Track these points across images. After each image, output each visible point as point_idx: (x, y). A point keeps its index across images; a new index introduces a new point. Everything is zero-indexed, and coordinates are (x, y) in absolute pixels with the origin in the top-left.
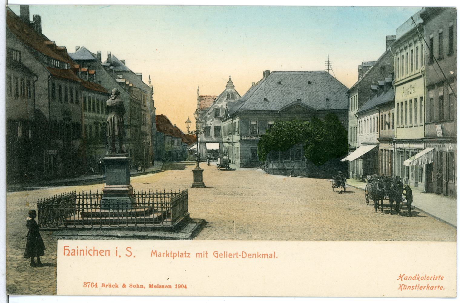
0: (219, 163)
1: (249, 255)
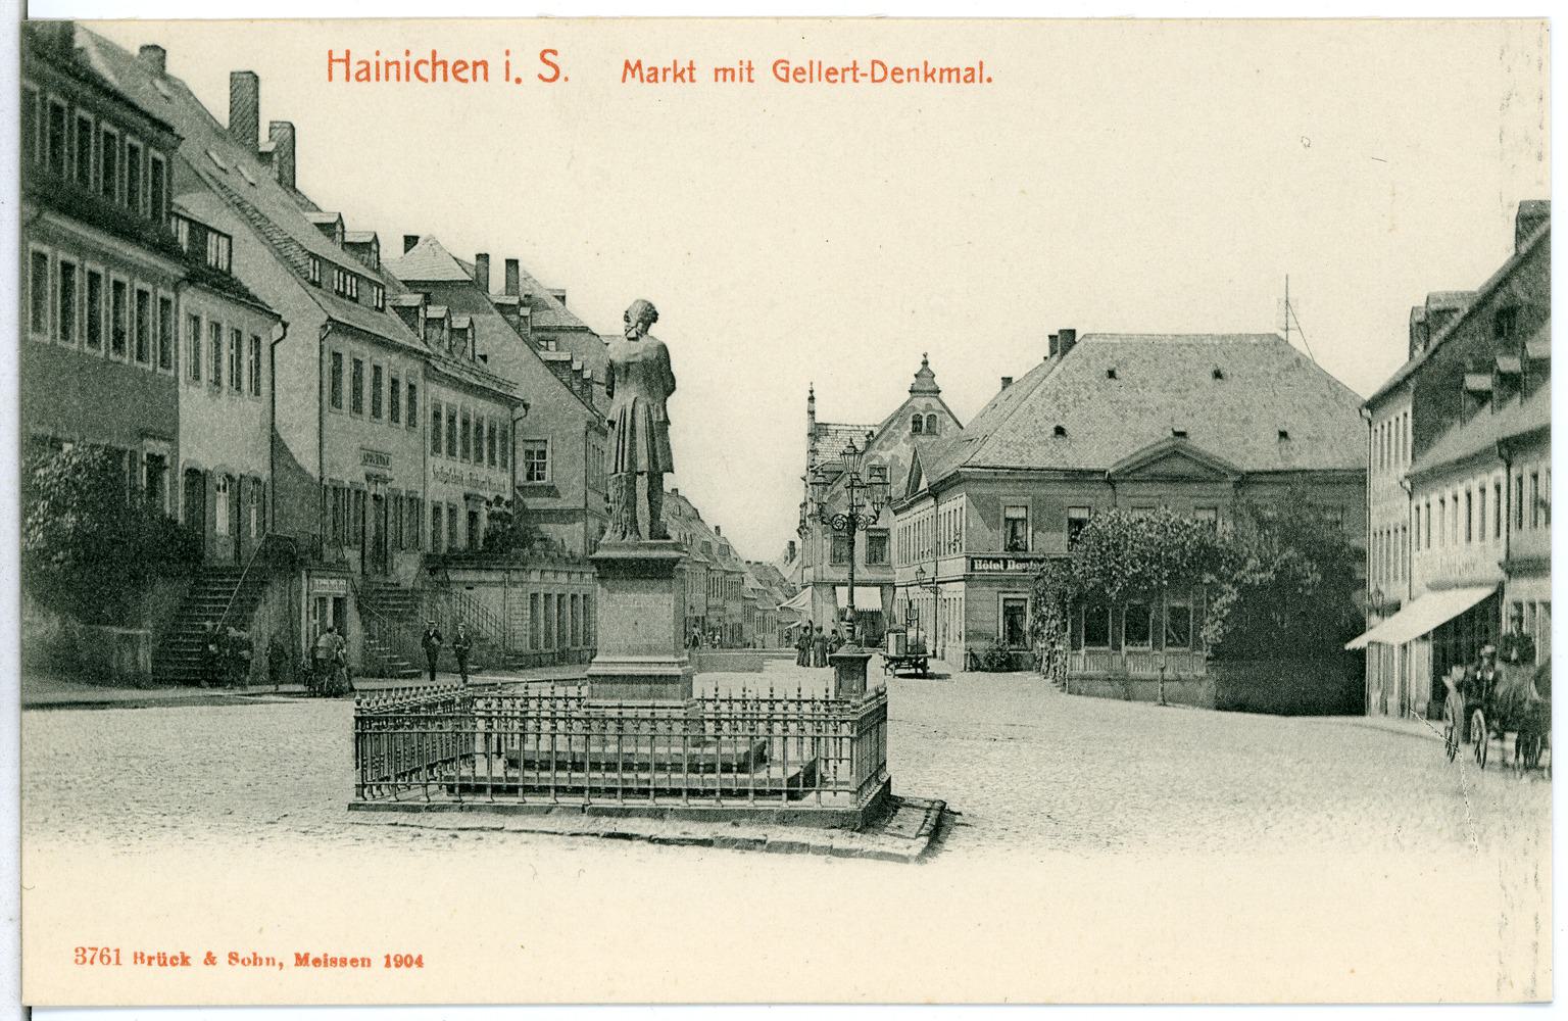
0: (892, 653)
1: (897, 71)
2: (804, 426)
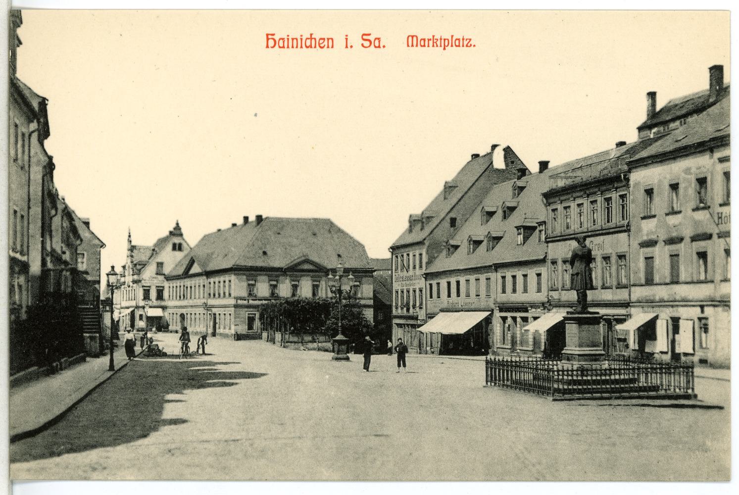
2: (126, 246)
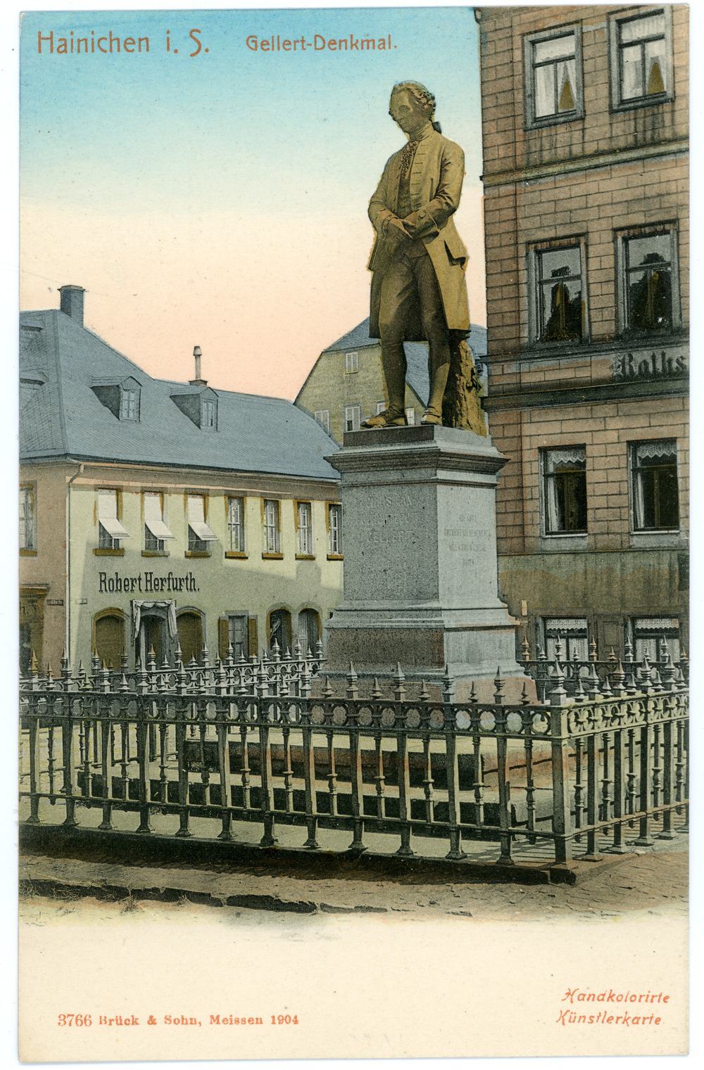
1: (333, 42)
